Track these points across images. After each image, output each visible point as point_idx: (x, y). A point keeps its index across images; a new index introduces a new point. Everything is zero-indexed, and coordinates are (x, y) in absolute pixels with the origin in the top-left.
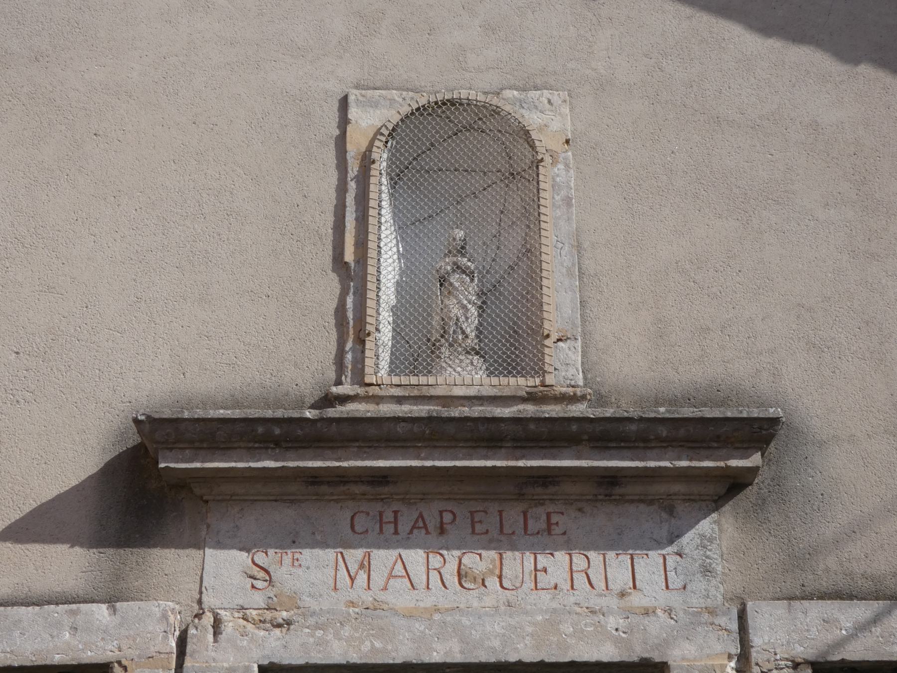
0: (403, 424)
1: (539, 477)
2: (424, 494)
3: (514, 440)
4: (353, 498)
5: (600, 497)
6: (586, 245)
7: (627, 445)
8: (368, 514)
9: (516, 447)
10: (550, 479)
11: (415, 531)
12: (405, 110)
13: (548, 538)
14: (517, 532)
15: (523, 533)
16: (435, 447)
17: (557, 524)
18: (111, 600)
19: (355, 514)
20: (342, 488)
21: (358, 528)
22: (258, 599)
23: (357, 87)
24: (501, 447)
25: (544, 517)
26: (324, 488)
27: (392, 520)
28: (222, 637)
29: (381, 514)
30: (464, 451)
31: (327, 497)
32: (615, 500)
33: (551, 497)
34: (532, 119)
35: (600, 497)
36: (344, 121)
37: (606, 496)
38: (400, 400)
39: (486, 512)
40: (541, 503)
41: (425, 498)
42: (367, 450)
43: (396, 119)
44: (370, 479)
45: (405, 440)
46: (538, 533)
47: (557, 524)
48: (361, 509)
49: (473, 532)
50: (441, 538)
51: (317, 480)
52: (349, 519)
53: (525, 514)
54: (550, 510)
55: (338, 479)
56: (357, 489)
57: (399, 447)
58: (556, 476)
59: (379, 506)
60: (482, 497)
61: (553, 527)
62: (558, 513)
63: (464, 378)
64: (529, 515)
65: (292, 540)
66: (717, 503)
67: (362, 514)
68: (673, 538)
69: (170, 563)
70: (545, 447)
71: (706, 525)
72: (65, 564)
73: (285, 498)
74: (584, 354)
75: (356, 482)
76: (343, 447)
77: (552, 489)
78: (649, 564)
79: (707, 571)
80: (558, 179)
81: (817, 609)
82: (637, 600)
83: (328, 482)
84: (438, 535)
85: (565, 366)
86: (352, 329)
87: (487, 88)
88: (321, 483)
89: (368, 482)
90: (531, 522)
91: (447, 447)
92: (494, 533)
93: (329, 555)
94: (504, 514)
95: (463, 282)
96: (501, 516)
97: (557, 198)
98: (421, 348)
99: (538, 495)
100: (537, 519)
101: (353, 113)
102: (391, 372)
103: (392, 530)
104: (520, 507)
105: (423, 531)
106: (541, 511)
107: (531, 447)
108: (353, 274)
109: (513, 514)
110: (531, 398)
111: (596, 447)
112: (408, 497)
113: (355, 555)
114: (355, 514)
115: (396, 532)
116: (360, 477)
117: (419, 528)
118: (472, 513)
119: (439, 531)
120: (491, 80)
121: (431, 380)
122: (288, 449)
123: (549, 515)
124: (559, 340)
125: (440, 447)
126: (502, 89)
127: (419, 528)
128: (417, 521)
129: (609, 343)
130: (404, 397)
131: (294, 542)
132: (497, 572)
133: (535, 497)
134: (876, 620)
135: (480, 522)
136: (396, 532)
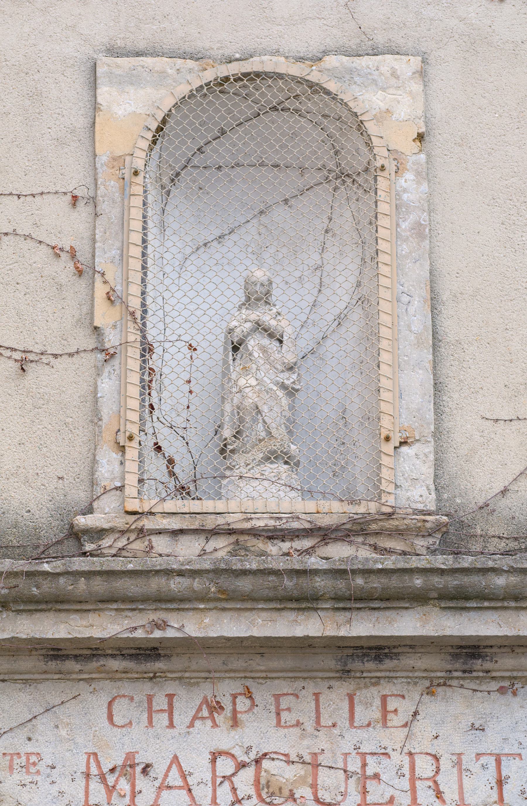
0: (178, 579)
1: (370, 648)
2: (209, 672)
3: (337, 598)
4: (113, 677)
5: (456, 674)
6: (445, 296)
7: (493, 604)
8: (132, 699)
9: (338, 609)
10: (387, 651)
11: (198, 723)
12: (184, 90)
14: (339, 723)
15: (347, 724)
16: (224, 609)
17: (396, 711)
19: (114, 699)
20: (94, 664)
21: (118, 719)
23: (113, 51)
24: (316, 609)
25: (377, 702)
26: (71, 665)
27: (166, 707)
29: (150, 699)
30: (264, 614)
31: (74, 676)
32: (477, 678)
33: (388, 674)
34: (369, 101)
35: (456, 674)
37: (464, 671)
39: (297, 696)
40: (376, 682)
41: (210, 676)
42: (130, 614)
43: (168, 103)
44: (134, 652)
45: (182, 600)
46: (369, 725)
47: (396, 711)
48: (122, 692)
49: (278, 724)
50: (233, 733)
51: (60, 653)
52: (106, 705)
53: (351, 698)
54: (386, 692)
55: (89, 652)
56: (115, 664)
57: (173, 609)
58: (394, 647)
59: (147, 688)
60: (291, 675)
61: (390, 716)
62: (397, 695)
64: (356, 700)
67: (123, 700)
70: (378, 609)
73: (17, 677)
74: (438, 463)
75: (113, 656)
76: (95, 610)
77: (388, 664)
80: (405, 196)
83: (76, 657)
87: (302, 50)
88: (67, 657)
89: (131, 655)
90: (358, 709)
91: (240, 609)
92: (309, 725)
94: (321, 699)
95: (264, 350)
96: (317, 701)
97: (404, 225)
99: (369, 671)
100: (368, 705)
103: (166, 723)
104: (342, 689)
105: (209, 723)
106: (374, 694)
107: (359, 609)
111: (450, 608)
112: (187, 675)
114: (114, 699)
115: (171, 725)
116: (119, 649)
117: (203, 718)
118: (277, 697)
119: (231, 723)
120: (309, 37)
121: (220, 506)
122: (19, 612)
123: (384, 699)
124: (403, 443)
125: (230, 609)
126: (326, 53)
127: (203, 718)
128: (200, 709)
130: (182, 532)
131: (29, 739)
132: (310, 780)
133: (365, 675)
135: (289, 709)
136: (171, 725)
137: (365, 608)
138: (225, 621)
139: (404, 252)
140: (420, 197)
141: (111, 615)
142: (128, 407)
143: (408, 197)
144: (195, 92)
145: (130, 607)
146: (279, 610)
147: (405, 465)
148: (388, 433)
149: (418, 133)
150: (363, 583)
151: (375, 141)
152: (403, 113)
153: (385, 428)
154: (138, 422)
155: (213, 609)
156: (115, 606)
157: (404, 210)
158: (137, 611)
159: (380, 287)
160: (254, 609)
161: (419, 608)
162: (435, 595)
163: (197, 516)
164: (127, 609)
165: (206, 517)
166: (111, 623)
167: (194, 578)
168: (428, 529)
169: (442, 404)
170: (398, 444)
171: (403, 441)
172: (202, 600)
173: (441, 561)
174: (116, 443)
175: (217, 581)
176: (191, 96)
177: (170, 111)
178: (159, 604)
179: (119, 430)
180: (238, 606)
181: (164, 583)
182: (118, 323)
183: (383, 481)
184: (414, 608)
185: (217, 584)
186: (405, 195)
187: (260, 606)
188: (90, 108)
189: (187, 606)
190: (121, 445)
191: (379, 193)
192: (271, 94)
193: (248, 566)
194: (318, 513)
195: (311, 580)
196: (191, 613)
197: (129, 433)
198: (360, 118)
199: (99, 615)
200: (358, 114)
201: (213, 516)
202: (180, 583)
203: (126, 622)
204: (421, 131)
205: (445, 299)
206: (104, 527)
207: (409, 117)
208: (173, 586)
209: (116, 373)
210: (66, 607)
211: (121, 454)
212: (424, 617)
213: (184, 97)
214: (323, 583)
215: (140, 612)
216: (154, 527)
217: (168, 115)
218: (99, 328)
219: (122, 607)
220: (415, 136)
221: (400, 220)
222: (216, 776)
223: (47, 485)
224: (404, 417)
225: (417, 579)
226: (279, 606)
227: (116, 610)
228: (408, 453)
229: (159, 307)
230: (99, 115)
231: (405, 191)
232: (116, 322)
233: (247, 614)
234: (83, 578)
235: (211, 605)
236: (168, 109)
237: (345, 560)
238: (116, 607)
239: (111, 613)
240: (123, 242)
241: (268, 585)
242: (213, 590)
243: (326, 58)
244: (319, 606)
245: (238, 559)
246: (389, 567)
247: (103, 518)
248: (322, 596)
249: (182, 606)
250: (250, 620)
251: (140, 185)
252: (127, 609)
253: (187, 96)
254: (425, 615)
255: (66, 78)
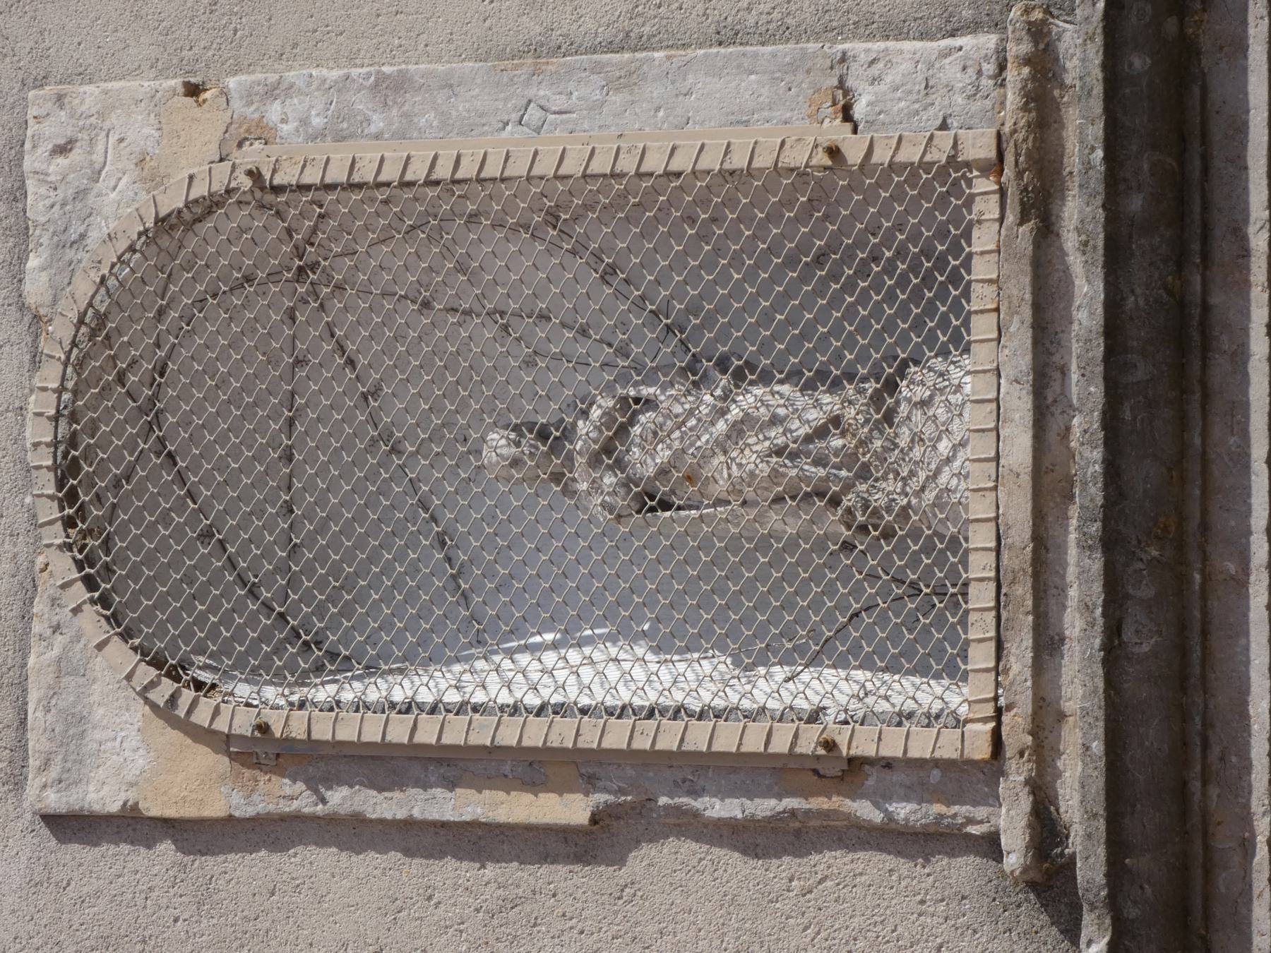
0: (1128, 634)
3: (1180, 262)
16: (1205, 527)
24: (1206, 308)
30: (1217, 431)
34: (120, 208)
42: (1215, 751)
43: (121, 655)
57: (1204, 648)
70: (1206, 158)
76: (1205, 834)
80: (317, 122)
107: (1206, 206)
121: (982, 538)
125: (1205, 512)
137: (1203, 189)
138: (1233, 523)
139: (435, 124)
140: (318, 89)
141: (1219, 796)
142: (762, 749)
143: (318, 115)
144: (96, 595)
145: (1198, 750)
146: (1206, 397)
147: (895, 109)
148: (820, 149)
149: (186, 95)
150: (1141, 196)
151: (199, 190)
152: (146, 131)
153: (810, 157)
154: (850, 727)
155: (1204, 552)
156: (1196, 786)
157: (345, 125)
158: (1210, 732)
159: (506, 174)
160: (1204, 454)
161: (1204, 62)
162: (1171, 25)
163: (1004, 591)
164: (1204, 757)
165: (1006, 571)
166: (1236, 797)
167: (1127, 596)
168: (1037, 50)
169: (764, 29)
170: (848, 126)
171: (840, 115)
172: (1182, 580)
173: (1088, 11)
174: (842, 778)
175: (1134, 542)
176: (104, 601)
177: (135, 649)
178: (1192, 681)
179: (816, 772)
180: (1198, 492)
181: (1138, 667)
182: (583, 771)
183: (928, 158)
184: (1204, 74)
185: (1139, 542)
186: (314, 123)
187: (1197, 441)
188: (134, 830)
189: (1197, 614)
190: (846, 768)
191: (307, 179)
192: (117, 428)
193: (1097, 467)
194: (997, 310)
195: (1131, 319)
196: (1214, 605)
197: (819, 748)
198: (150, 224)
199: (1219, 824)
200: (141, 229)
201: (1005, 555)
202: (1137, 632)
203: (1234, 759)
204: (181, 90)
205: (538, 29)
206: (1028, 809)
207: (152, 116)
208: (1145, 648)
209: (690, 777)
210: (1197, 901)
211: (867, 767)
212: (1226, 49)
213: (107, 618)
214: (1138, 291)
215: (1212, 726)
216: (1029, 693)
217: (144, 654)
218: (593, 814)
219: (1198, 768)
220: (190, 101)
221: (366, 132)
222: (92, 329)
223: (939, 940)
224: (788, 115)
225: (1131, 65)
226: (1198, 396)
227: (1205, 783)
228: (869, 104)
229: (573, 677)
230: (148, 810)
231: (305, 122)
232: (582, 775)
233: (1216, 471)
234: (1127, 861)
235: (1193, 556)
236: (132, 653)
237: (1083, 237)
238: (1198, 784)
239: (1215, 797)
240: (410, 759)
241: (1142, 420)
242: (1155, 553)
243: (31, 301)
244: (1199, 301)
245: (1081, 492)
246: (1101, 133)
247: (1009, 810)
248: (1170, 293)
249: (1197, 627)
250: (1230, 464)
251: (288, 717)
252: (1204, 757)
253: (105, 612)
254: (1221, 48)
255: (73, 884)
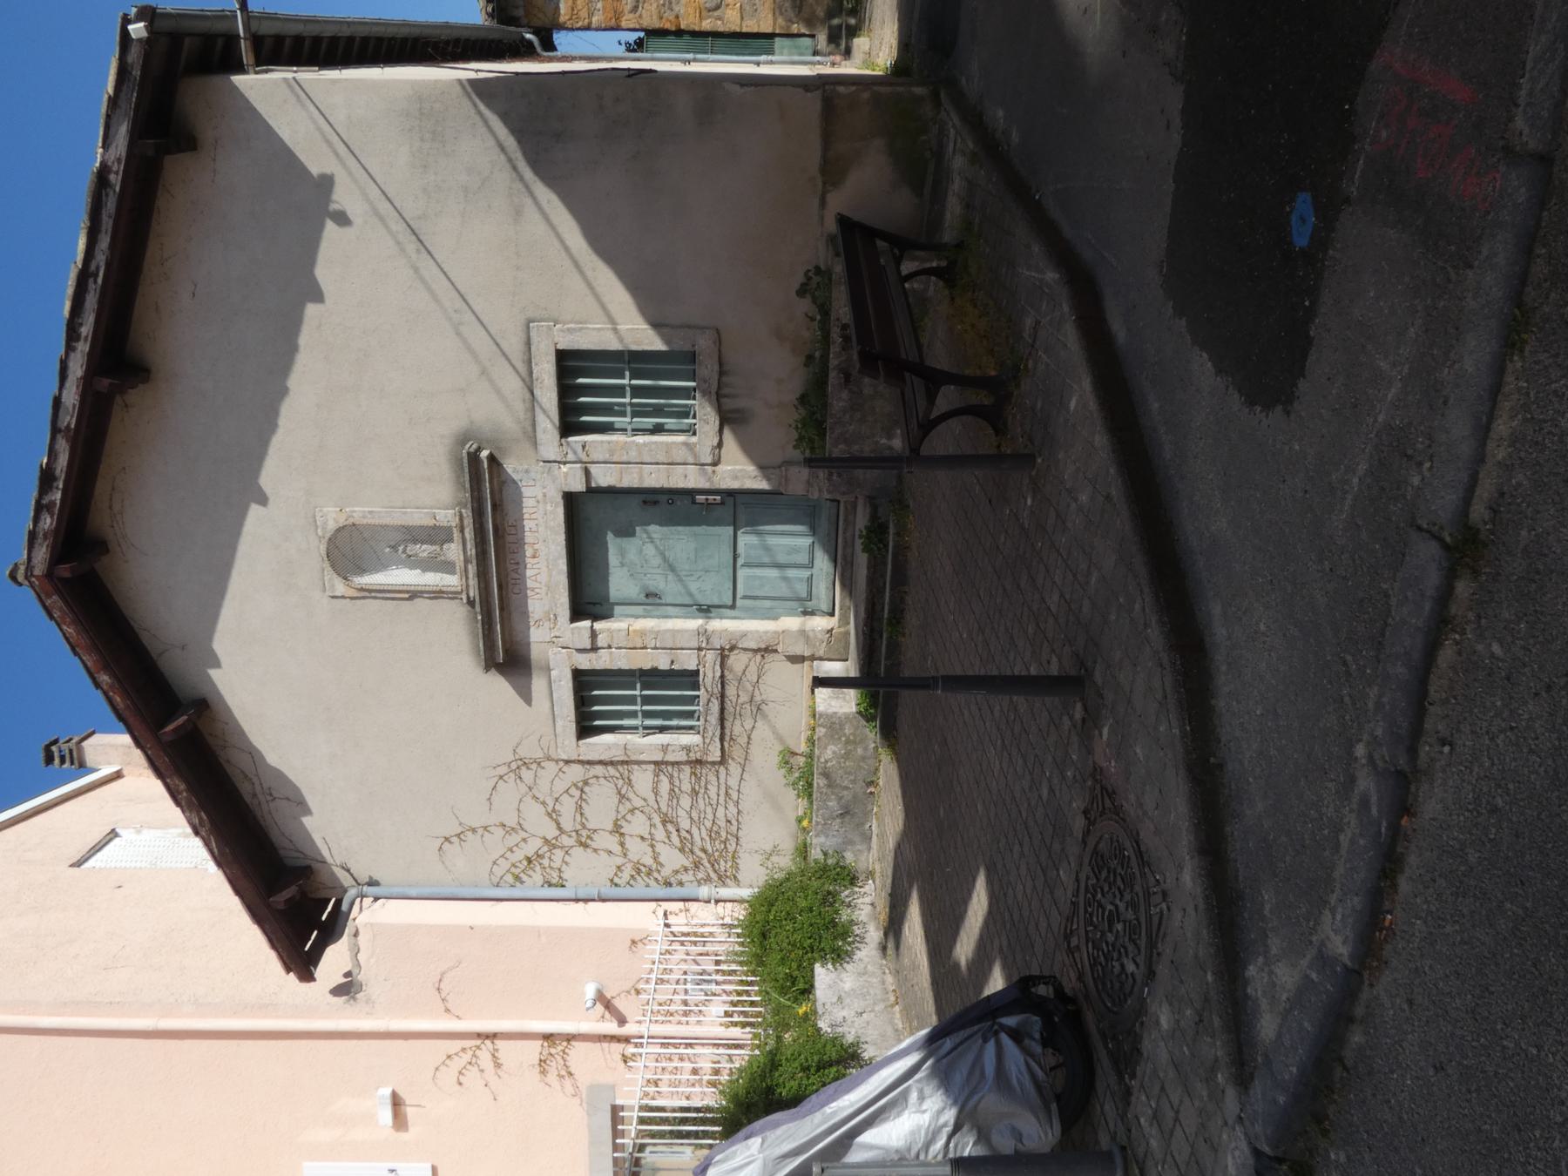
13: (518, 527)
18: (549, 670)
22: (547, 624)
28: (630, 80)
34: (332, 526)
36: (343, 597)
38: (674, 1110)
63: (453, 551)
65: (525, 614)
66: (499, 465)
68: (514, 482)
69: (536, 652)
71: (509, 471)
72: (538, 684)
78: (526, 492)
79: (527, 471)
81: (540, 435)
82: (540, 497)
84: (520, 565)
85: (447, 517)
86: (438, 594)
93: (530, 601)
98: (447, 567)
101: (338, 594)
102: (453, 572)
108: (413, 594)
109: (510, 539)
110: (462, 531)
113: (529, 593)
129: (437, 499)
134: (544, 411)
